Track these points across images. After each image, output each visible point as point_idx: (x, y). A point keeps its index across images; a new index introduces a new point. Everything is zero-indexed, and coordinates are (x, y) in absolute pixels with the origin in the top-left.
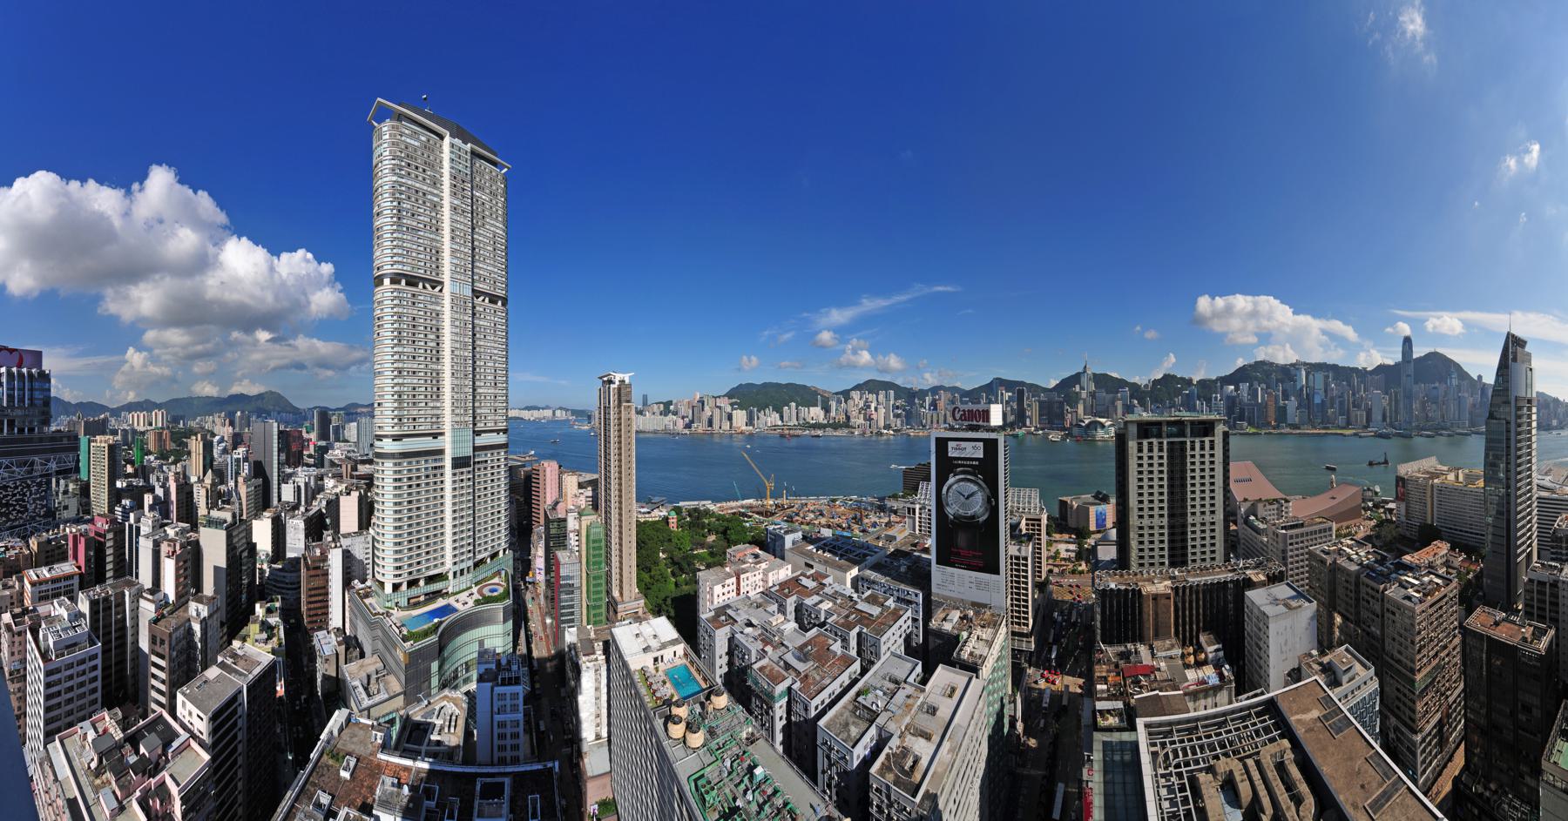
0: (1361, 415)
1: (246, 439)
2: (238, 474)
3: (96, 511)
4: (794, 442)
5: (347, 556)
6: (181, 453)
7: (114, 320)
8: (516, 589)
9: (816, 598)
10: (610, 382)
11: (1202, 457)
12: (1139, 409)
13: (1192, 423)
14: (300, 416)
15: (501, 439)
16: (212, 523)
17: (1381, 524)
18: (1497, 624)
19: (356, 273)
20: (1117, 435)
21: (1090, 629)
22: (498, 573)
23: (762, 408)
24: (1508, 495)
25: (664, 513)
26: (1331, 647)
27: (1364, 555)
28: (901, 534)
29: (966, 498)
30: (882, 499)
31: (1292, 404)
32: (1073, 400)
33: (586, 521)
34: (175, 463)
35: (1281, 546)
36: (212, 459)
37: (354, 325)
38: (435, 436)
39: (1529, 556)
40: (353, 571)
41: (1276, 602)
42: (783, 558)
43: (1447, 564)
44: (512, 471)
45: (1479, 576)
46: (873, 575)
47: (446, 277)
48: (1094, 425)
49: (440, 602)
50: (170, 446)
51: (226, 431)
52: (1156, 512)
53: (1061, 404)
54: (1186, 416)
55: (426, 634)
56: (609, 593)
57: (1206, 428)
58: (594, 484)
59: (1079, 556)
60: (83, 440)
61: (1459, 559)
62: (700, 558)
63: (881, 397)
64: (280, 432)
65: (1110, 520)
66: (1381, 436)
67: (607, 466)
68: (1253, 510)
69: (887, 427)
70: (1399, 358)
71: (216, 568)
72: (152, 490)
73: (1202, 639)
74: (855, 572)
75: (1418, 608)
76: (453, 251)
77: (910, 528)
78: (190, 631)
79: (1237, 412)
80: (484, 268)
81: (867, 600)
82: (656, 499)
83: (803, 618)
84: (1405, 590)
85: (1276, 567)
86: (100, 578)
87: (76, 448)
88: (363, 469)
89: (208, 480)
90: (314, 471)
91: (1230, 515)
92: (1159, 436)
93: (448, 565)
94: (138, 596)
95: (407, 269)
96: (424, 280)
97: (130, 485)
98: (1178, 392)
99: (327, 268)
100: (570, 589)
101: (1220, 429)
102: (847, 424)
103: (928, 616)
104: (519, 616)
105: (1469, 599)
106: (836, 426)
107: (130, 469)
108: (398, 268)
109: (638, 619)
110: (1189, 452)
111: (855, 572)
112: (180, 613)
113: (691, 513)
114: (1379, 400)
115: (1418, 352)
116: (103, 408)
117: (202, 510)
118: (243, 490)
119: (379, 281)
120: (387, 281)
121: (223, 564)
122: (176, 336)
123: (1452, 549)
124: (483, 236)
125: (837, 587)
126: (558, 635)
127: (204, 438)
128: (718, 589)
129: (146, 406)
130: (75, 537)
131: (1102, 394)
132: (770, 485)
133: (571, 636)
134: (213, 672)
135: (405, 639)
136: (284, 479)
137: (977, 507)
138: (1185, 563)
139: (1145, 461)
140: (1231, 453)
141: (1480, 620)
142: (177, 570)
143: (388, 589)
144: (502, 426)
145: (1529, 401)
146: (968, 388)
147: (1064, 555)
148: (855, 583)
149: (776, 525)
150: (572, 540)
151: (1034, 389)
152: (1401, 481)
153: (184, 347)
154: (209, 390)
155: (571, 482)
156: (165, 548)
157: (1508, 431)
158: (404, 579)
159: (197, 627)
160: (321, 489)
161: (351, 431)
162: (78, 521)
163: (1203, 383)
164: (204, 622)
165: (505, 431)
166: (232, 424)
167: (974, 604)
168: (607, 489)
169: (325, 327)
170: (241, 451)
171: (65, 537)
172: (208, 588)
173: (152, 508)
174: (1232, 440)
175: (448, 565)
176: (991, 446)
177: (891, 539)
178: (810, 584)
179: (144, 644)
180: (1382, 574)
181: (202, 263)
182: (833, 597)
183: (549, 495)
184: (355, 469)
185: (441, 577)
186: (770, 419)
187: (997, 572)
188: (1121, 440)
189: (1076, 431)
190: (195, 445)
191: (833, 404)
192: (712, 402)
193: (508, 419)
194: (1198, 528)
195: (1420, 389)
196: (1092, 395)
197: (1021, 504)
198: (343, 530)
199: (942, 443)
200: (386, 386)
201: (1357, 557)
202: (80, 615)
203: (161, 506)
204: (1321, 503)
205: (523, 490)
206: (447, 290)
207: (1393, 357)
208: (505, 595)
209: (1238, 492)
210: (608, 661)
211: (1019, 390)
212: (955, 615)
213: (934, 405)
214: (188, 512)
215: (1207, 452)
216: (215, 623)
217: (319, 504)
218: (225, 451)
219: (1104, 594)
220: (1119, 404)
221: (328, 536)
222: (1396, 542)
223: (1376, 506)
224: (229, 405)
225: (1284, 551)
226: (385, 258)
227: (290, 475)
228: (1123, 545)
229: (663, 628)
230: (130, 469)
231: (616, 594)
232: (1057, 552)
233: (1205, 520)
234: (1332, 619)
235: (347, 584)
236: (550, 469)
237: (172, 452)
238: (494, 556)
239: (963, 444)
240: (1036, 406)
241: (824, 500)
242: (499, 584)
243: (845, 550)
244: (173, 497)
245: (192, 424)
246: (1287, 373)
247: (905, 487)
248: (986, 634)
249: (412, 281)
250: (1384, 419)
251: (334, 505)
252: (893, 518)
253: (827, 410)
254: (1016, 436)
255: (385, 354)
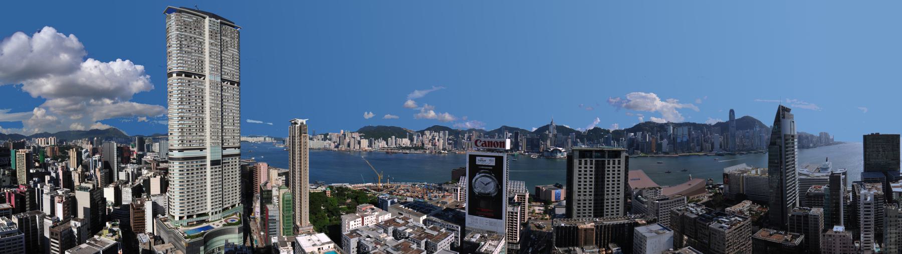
0: (709, 145)
1: (99, 151)
2: (95, 167)
3: (20, 183)
4: (393, 155)
5: (155, 205)
6: (65, 157)
7: (27, 94)
8: (245, 221)
9: (404, 228)
10: (296, 123)
11: (613, 169)
12: (580, 144)
13: (609, 151)
14: (128, 140)
15: (237, 151)
16: (81, 189)
17: (716, 194)
18: (771, 235)
19: (158, 73)
20: (568, 156)
21: (551, 243)
22: (236, 214)
23: (377, 138)
24: (781, 179)
25: (324, 189)
26: (681, 247)
27: (700, 211)
28: (450, 201)
29: (485, 185)
30: (440, 185)
31: (665, 142)
32: (544, 138)
33: (282, 191)
34: (61, 162)
35: (656, 208)
36: (82, 160)
37: (157, 95)
38: (201, 150)
39: (794, 205)
40: (157, 210)
41: (651, 231)
42: (387, 210)
43: (750, 210)
44: (243, 167)
45: (767, 214)
46: (434, 219)
47: (207, 72)
48: (556, 151)
49: (205, 225)
50: (58, 154)
51: (89, 147)
52: (588, 193)
53: (538, 140)
54: (605, 148)
55: (197, 236)
56: (294, 223)
57: (616, 154)
58: (286, 174)
59: (545, 212)
60: (13, 152)
61: (756, 208)
62: (343, 210)
63: (441, 134)
64: (118, 148)
65: (563, 196)
66: (719, 155)
67: (294, 166)
68: (640, 193)
69: (444, 149)
70: (728, 119)
71: (85, 208)
72: (49, 174)
73: (610, 245)
74: (425, 217)
75: (727, 232)
76: (210, 62)
77: (457, 196)
78: (72, 232)
79: (633, 146)
80: (226, 69)
81: (431, 229)
82: (319, 182)
83: (396, 235)
84: (720, 225)
85: (651, 218)
86: (23, 210)
87: (9, 155)
88: (162, 165)
89: (80, 169)
90: (136, 166)
91: (628, 194)
92: (591, 157)
93: (209, 209)
94: (44, 216)
95: (186, 69)
96: (195, 74)
97: (37, 171)
98: (602, 136)
99: (140, 68)
100: (274, 221)
101: (624, 155)
102: (422, 147)
103: (463, 234)
104: (246, 231)
105: (759, 222)
106: (416, 148)
107: (37, 164)
108: (180, 69)
109: (309, 233)
110: (607, 166)
111: (425, 217)
112: (66, 224)
113: (338, 189)
114: (718, 139)
115: (738, 116)
116: (23, 137)
117: (77, 183)
118: (98, 175)
119: (170, 75)
120: (174, 75)
121: (88, 206)
122: (61, 102)
123: (753, 203)
124: (227, 55)
125: (415, 223)
126: (267, 239)
127: (77, 150)
128: (352, 223)
129: (46, 135)
130: (9, 194)
131: (560, 136)
132: (381, 177)
133: (274, 240)
134: (84, 246)
135: (186, 238)
136: (120, 169)
137: (491, 188)
138: (602, 216)
139: (583, 169)
140: (630, 166)
141: (762, 234)
142: (64, 208)
143: (177, 218)
144: (237, 145)
145: (793, 136)
146: (489, 130)
147: (537, 211)
148: (425, 222)
149: (384, 195)
150: (275, 200)
151: (524, 132)
152: (726, 176)
153: (65, 106)
154: (80, 127)
155: (274, 173)
156: (57, 199)
157: (781, 151)
158: (185, 215)
159: (75, 230)
160: (140, 174)
161: (156, 147)
162: (10, 187)
163: (616, 132)
164: (78, 229)
165: (239, 148)
166: (92, 143)
167: (487, 232)
168: (294, 177)
169: (139, 97)
170: (97, 157)
171: (4, 193)
172: (81, 215)
173: (49, 182)
174: (630, 160)
175: (209, 209)
176: (499, 160)
177: (444, 203)
178: (401, 222)
179: (47, 234)
180: (709, 218)
181: (73, 68)
182: (413, 227)
183: (262, 179)
184: (158, 165)
185: (205, 214)
186: (381, 144)
187: (501, 218)
188: (570, 158)
189: (545, 154)
190: (73, 154)
191: (415, 137)
192: (350, 135)
193: (240, 142)
194: (610, 201)
195: (740, 133)
196: (555, 136)
197: (514, 188)
198: (152, 193)
199: (473, 158)
200: (174, 125)
201: (695, 211)
202: (13, 224)
203: (55, 181)
204: (683, 188)
205: (248, 177)
206: (207, 79)
207: (725, 119)
208: (240, 222)
209: (632, 185)
210: (294, 249)
211: (516, 133)
212: (478, 236)
213: (470, 138)
214: (68, 182)
215: (616, 165)
216: (85, 228)
217: (139, 181)
218: (88, 156)
219: (558, 228)
220: (570, 141)
221: (144, 196)
222: (719, 204)
223: (714, 187)
224: (90, 135)
225: (657, 210)
226: (173, 64)
227: (124, 168)
228: (569, 207)
229: (323, 237)
230: (37, 164)
231: (298, 224)
232: (534, 210)
233: (614, 196)
234: (682, 239)
235: (155, 215)
236: (263, 167)
237: (60, 157)
238: (233, 206)
239: (484, 158)
240: (525, 141)
241: (409, 184)
242: (236, 218)
243: (419, 207)
244: (61, 177)
245: (71, 144)
246: (662, 127)
247: (453, 178)
248: (494, 243)
249: (188, 75)
250: (721, 147)
251: (147, 182)
252: (446, 193)
253: (412, 140)
254: (513, 155)
255: (174, 109)
